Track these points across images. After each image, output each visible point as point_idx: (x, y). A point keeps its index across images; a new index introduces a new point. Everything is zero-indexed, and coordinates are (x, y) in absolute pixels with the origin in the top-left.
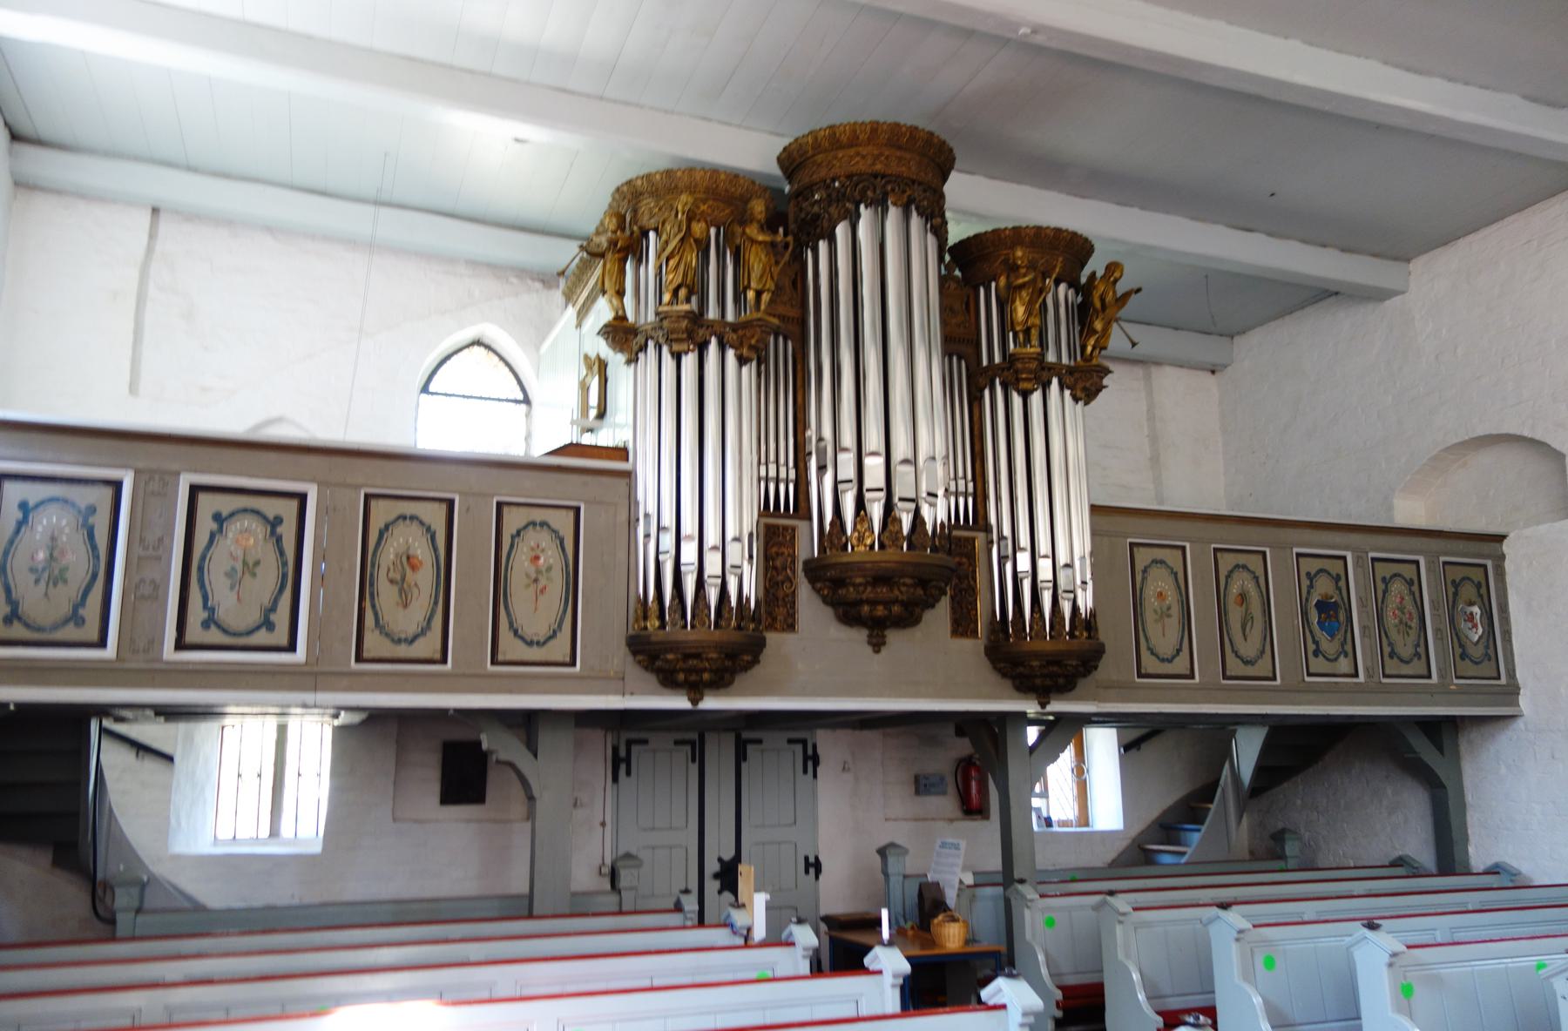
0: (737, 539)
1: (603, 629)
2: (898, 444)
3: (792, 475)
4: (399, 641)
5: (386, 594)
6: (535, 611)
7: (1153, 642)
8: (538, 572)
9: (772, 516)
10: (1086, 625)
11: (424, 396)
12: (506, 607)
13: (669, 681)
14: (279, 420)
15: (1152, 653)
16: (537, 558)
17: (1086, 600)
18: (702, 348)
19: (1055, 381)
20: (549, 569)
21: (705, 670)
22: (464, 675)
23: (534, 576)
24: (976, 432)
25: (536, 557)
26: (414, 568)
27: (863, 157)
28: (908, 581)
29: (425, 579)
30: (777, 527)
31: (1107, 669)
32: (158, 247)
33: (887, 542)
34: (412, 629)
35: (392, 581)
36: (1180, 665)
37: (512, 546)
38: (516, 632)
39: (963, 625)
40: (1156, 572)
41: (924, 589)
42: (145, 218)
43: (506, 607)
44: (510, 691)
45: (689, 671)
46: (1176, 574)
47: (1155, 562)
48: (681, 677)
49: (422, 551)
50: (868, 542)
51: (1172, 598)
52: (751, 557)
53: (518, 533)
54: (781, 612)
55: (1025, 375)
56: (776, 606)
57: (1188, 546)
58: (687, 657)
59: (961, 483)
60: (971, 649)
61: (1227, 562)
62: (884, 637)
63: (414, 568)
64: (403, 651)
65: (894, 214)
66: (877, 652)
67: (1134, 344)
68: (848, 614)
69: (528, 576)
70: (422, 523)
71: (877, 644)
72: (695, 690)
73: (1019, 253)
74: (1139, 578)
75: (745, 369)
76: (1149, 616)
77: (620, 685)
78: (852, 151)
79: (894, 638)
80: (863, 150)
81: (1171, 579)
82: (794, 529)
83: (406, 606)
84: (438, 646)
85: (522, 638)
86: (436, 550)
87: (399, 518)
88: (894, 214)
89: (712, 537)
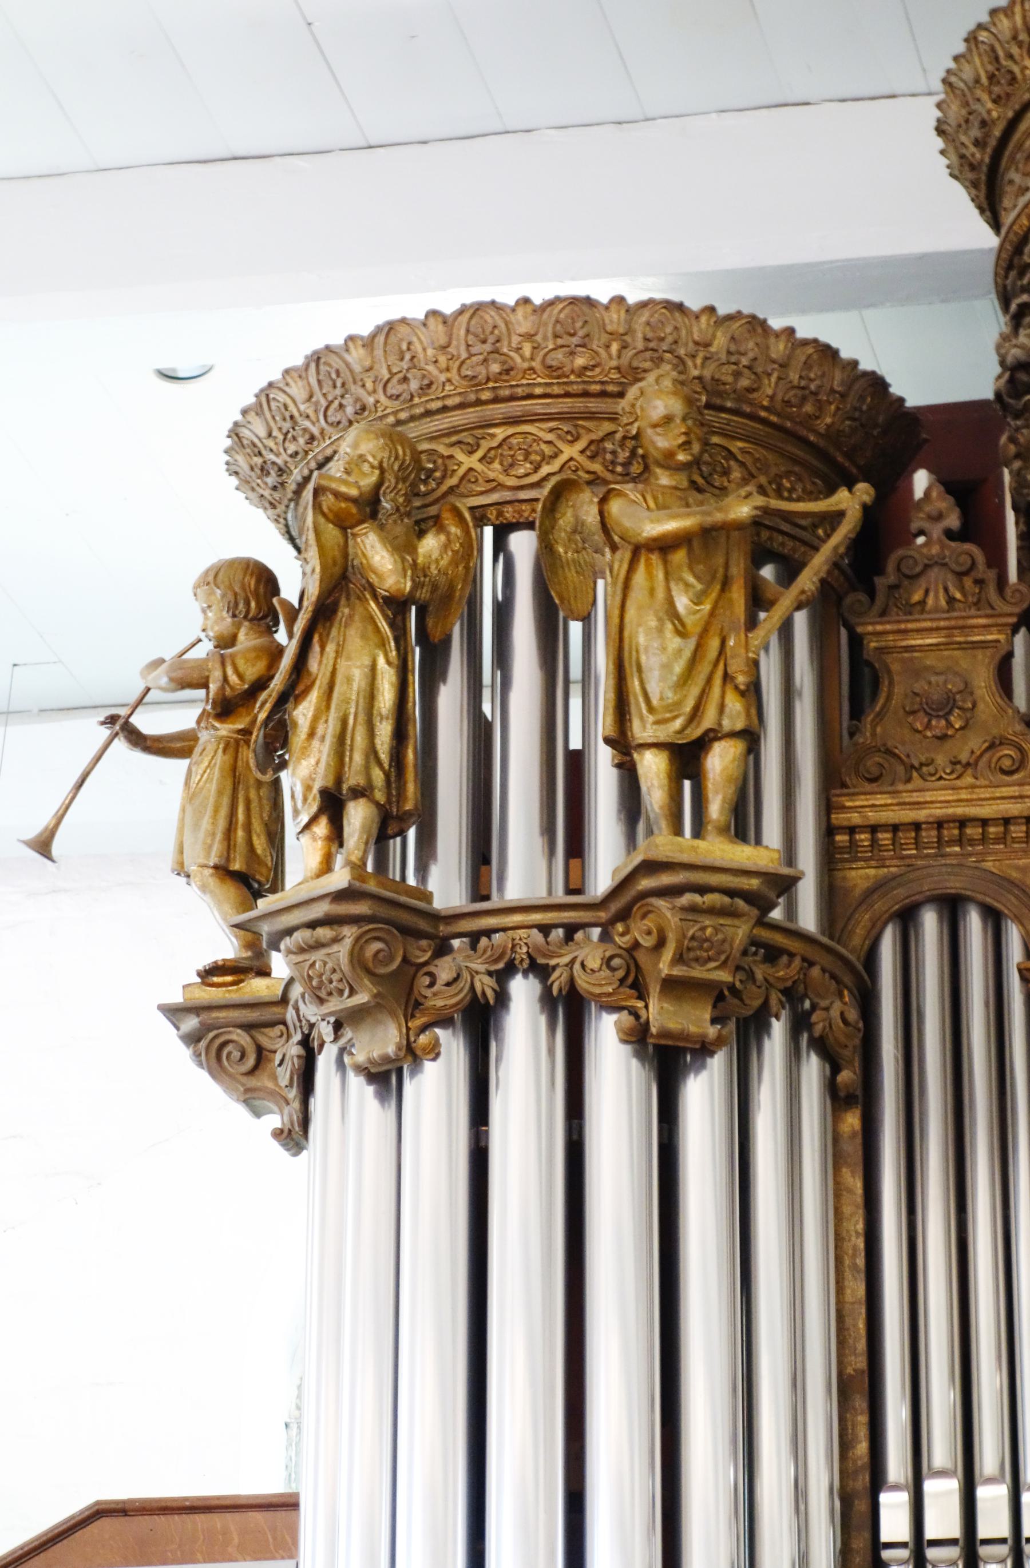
71: (173, 1012)
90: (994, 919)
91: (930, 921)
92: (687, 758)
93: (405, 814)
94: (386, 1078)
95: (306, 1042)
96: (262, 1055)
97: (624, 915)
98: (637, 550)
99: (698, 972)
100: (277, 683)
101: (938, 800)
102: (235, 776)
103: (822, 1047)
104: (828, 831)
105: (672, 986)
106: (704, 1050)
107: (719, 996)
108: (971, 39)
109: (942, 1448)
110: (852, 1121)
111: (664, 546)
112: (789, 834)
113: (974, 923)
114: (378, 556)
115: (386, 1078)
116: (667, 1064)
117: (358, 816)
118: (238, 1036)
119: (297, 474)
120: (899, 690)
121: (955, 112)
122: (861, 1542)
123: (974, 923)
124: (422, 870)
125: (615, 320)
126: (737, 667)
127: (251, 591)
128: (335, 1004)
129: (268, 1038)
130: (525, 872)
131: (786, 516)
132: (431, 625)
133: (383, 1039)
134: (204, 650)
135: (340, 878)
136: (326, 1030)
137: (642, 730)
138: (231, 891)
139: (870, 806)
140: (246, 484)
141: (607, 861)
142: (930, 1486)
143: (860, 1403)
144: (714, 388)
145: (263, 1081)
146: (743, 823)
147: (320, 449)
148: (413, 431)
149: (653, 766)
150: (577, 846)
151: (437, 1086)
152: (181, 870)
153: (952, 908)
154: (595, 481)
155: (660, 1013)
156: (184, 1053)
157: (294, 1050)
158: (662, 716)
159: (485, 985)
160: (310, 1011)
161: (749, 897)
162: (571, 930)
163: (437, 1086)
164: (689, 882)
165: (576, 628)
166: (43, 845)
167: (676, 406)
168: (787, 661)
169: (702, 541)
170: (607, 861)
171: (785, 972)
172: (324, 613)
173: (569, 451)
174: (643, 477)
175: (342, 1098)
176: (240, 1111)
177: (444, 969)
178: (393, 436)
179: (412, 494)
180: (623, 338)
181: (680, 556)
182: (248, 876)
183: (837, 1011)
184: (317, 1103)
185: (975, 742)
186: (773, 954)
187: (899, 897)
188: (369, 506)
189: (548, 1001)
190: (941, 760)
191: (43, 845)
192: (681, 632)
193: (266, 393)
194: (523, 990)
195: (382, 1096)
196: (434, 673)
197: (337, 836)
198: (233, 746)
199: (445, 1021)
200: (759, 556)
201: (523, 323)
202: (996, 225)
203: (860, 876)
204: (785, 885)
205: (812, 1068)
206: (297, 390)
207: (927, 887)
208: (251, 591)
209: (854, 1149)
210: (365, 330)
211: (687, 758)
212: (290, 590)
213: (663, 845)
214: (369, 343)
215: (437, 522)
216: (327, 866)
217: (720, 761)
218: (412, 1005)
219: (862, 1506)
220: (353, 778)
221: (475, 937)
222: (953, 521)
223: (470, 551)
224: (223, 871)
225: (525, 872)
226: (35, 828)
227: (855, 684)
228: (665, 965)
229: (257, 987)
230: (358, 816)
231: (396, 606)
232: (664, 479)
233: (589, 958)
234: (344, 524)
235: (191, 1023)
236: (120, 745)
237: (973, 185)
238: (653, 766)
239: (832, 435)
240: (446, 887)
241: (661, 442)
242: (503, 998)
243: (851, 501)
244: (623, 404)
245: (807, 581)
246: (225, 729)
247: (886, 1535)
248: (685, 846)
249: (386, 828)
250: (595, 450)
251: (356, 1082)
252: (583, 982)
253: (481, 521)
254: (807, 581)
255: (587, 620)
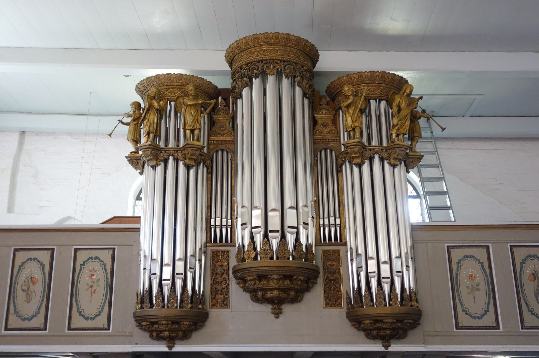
0: (399, 257)
1: (125, 308)
2: (269, 202)
3: (338, 222)
4: (25, 319)
5: (20, 295)
6: (91, 301)
7: (467, 306)
8: (93, 282)
9: (325, 244)
10: (409, 298)
11: (137, 201)
12: (76, 301)
13: (158, 337)
14: (69, 218)
15: (466, 314)
16: (93, 275)
17: (409, 282)
18: (371, 160)
19: (376, 156)
20: (98, 280)
21: (387, 329)
22: (53, 336)
23: (90, 284)
24: (340, 190)
25: (94, 274)
26: (34, 283)
27: (252, 53)
28: (275, 277)
29: (38, 289)
30: (218, 251)
31: (428, 324)
32: (25, 147)
33: (280, 256)
34: (31, 314)
35: (23, 290)
36: (489, 320)
37: (81, 270)
38: (80, 313)
39: (332, 299)
40: (466, 263)
41: (291, 281)
42: (16, 137)
43: (76, 301)
44: (76, 344)
45: (379, 329)
46: (105, 265)
47: (466, 257)
48: (375, 332)
49: (38, 275)
50: (270, 255)
51: (480, 278)
52: (408, 266)
53: (84, 264)
54: (220, 297)
55: (362, 154)
56: (220, 295)
57: (490, 245)
58: (376, 322)
59: (224, 220)
60: (339, 314)
61: (520, 254)
62: (281, 309)
63: (34, 283)
64: (26, 324)
65: (271, 80)
66: (277, 318)
67: (443, 129)
68: (258, 296)
69: (87, 284)
70: (39, 261)
71: (277, 314)
72: (386, 340)
73: (346, 89)
74: (454, 267)
75: (396, 170)
76: (463, 290)
77: (127, 338)
78: (247, 52)
79: (287, 309)
80: (252, 50)
81: (479, 267)
82: (228, 252)
83: (29, 302)
84: (43, 321)
85: (83, 316)
86: (44, 274)
87: (28, 259)
88: (271, 80)
89: (384, 257)
90: (227, 152)
91: (220, 152)
92: (192, 131)
93: (157, 135)
94: (154, 167)
95: (144, 162)
96: (138, 163)
97: (184, 150)
98: (187, 105)
99: (193, 157)
100: (142, 118)
101: (222, 138)
102: (135, 129)
103: (207, 167)
104: (208, 141)
105: (189, 158)
106: (193, 166)
107: (195, 160)
108: (230, 46)
109: (219, 214)
110: (210, 175)
111: (191, 105)
112: (203, 141)
113: (225, 153)
114: (155, 104)
115: (154, 167)
116: (188, 168)
117: (151, 135)
118: (135, 160)
119: (144, 92)
120: (217, 124)
121: (227, 55)
122: (209, 225)
123: (225, 153)
124: (159, 142)
125: (185, 77)
126: (199, 121)
127: (137, 106)
128: (148, 158)
129: (139, 161)
130: (172, 143)
131: (206, 103)
132: (161, 112)
133: (154, 163)
134: (132, 113)
135: (149, 143)
136: (146, 161)
137: (187, 128)
138: (134, 143)
139: (213, 138)
140: (137, 92)
141: (182, 144)
142: (217, 219)
143: (209, 209)
144: (197, 86)
145: (138, 166)
146: (198, 140)
147: (147, 89)
148: (160, 88)
149: (188, 132)
150: (178, 140)
151: (160, 169)
152: (128, 139)
153: (223, 151)
154: (182, 96)
155: (188, 162)
156: (128, 162)
157: (142, 163)
158: (190, 126)
159: (167, 157)
160: (144, 158)
161: (199, 149)
162: (177, 151)
163: (160, 169)
164: (192, 146)
165: (179, 114)
166: (110, 135)
167: (193, 88)
168: (204, 120)
169: (195, 105)
170: (182, 144)
171: (203, 157)
172: (148, 110)
173: (179, 92)
174: (188, 97)
175: (148, 169)
176: (135, 170)
177: (162, 155)
178: (157, 89)
179: (159, 96)
180: (186, 79)
181: (192, 107)
182: (136, 141)
183: (208, 162)
184: (144, 170)
185: (226, 131)
186: (201, 155)
187: (216, 149)
188: (154, 97)
189: (174, 159)
190: (222, 133)
191: (110, 135)
192: (192, 116)
193: (141, 82)
194: (171, 158)
195: (153, 169)
196: (161, 118)
197: (149, 137)
198: (135, 125)
199: (161, 161)
200: (202, 107)
201: (174, 76)
202: (231, 69)
203: (212, 146)
204: (203, 147)
205: (205, 169)
206: (145, 82)
207: (220, 148)
208: (137, 106)
209: (210, 179)
210: (154, 75)
211: (192, 131)
212: (143, 106)
213: (189, 142)
214: (154, 77)
215: (162, 100)
216: (147, 142)
217: (196, 132)
218: (157, 159)
219: (209, 221)
220: (151, 131)
221: (165, 151)
222: (225, 104)
223: (166, 104)
224: (133, 140)
225: (172, 143)
226: (109, 133)
227: (212, 123)
228: (189, 156)
229: (137, 155)
230: (151, 135)
231: (157, 110)
232: (191, 97)
233: (179, 155)
234: (151, 100)
235: (129, 159)
236: (120, 124)
237: (229, 64)
238: (188, 132)
239: (211, 93)
240: (162, 145)
241: (191, 93)
242: (169, 159)
243: (213, 102)
244: (186, 88)
245: (208, 111)
246: (134, 123)
247: (212, 224)
248: (191, 142)
249: (155, 137)
250: (182, 93)
251: (150, 167)
252: (179, 157)
253: (168, 100)
254: (208, 111)
255: (180, 114)
